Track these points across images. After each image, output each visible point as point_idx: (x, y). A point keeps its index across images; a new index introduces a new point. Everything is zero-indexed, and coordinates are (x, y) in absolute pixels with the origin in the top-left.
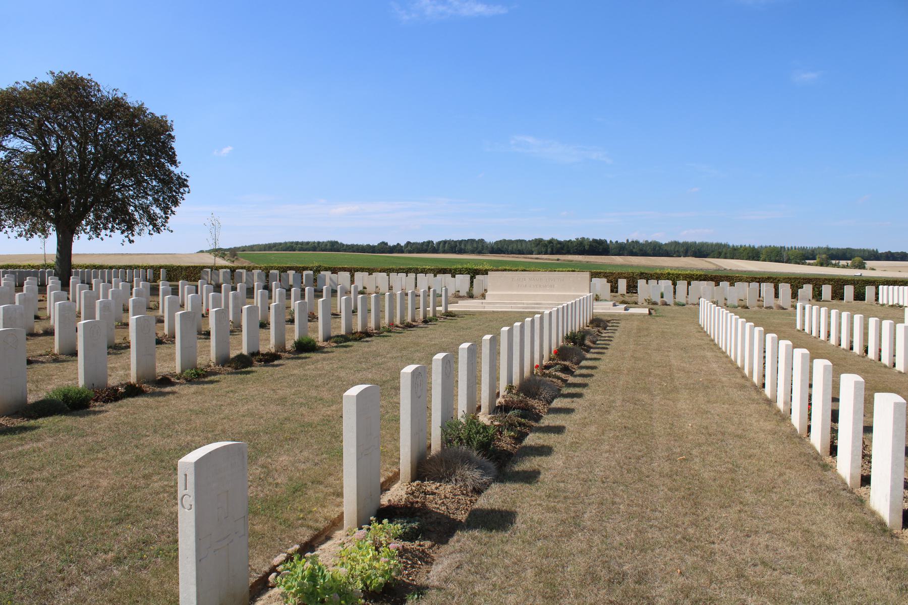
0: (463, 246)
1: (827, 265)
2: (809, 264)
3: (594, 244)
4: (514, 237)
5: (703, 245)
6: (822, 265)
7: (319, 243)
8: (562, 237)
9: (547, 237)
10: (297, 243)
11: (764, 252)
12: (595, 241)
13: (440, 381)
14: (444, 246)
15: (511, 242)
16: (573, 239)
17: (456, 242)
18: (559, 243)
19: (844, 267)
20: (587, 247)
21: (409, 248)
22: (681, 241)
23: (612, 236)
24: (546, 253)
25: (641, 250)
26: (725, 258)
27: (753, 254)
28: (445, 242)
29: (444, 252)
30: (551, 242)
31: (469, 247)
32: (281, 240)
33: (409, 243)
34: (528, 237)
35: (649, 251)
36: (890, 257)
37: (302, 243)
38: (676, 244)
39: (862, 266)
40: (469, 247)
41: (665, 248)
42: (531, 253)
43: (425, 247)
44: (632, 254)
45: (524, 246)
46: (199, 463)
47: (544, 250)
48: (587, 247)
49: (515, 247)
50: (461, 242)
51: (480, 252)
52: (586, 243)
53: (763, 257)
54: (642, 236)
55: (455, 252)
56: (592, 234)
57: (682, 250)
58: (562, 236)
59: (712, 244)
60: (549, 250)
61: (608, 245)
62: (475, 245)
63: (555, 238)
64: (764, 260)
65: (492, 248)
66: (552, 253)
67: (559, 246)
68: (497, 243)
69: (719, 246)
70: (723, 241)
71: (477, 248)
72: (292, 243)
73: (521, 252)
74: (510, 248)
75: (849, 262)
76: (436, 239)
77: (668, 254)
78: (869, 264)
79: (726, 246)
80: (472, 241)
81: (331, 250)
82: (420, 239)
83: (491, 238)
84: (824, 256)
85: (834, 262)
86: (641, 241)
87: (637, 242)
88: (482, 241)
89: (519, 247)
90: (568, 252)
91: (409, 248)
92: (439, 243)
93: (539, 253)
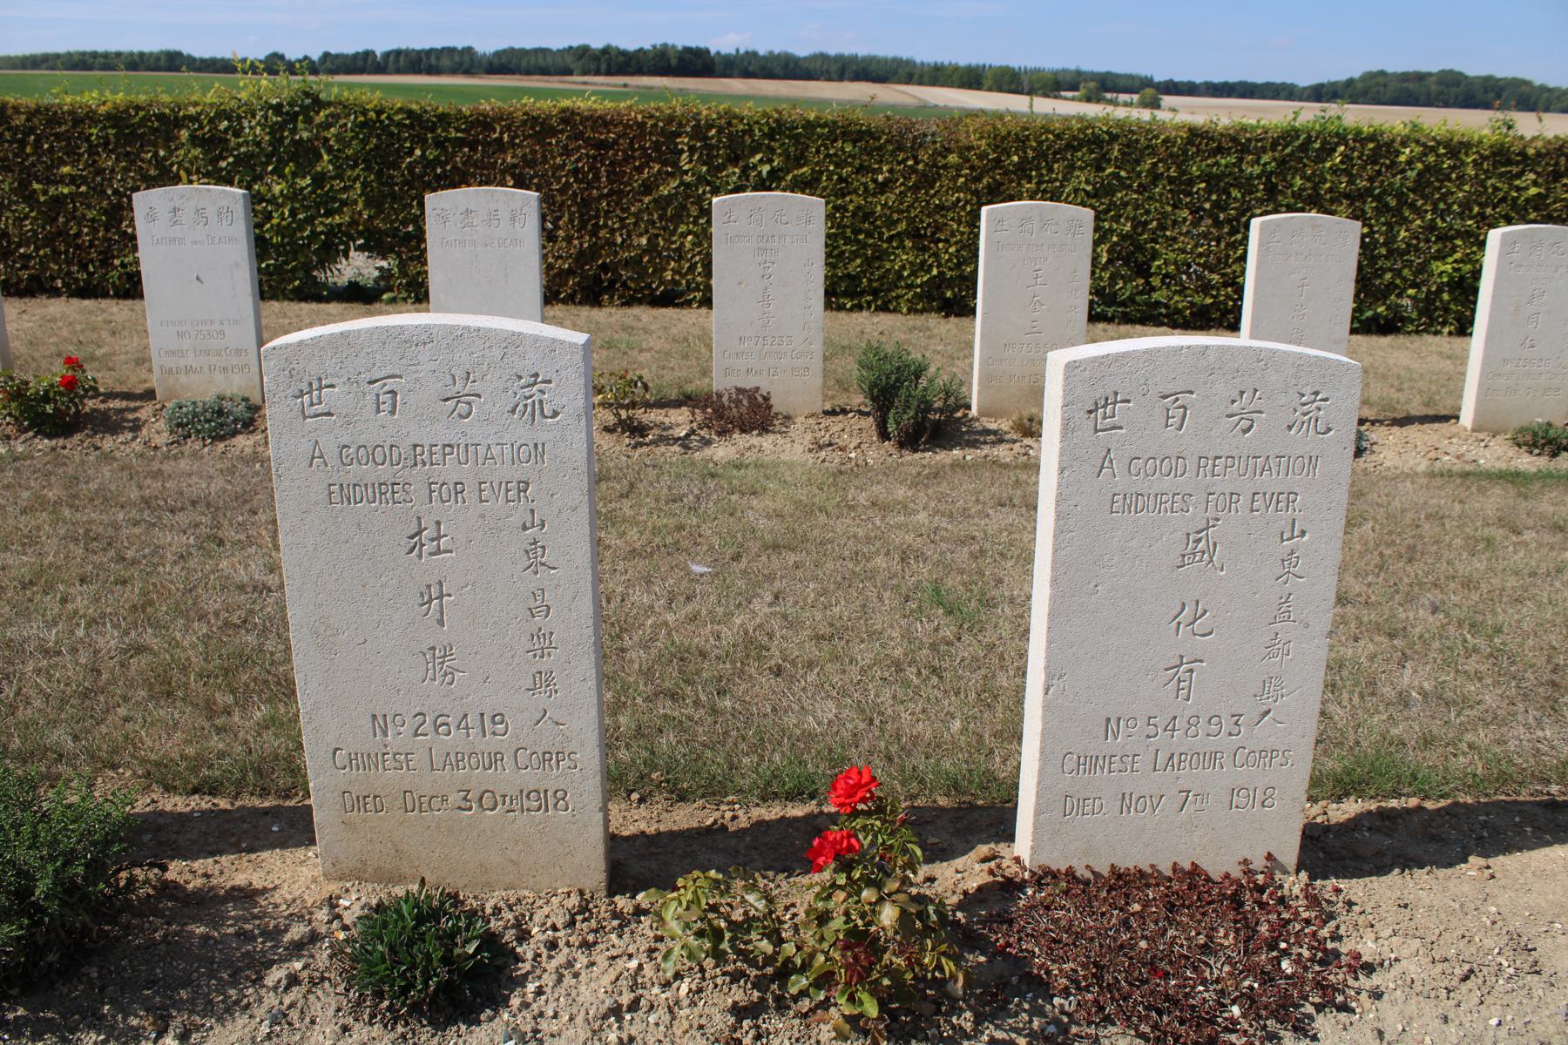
0: (433, 61)
1: (1098, 101)
2: (1066, 99)
3: (687, 56)
4: (529, 44)
5: (871, 60)
6: (1088, 100)
7: (142, 54)
8: (629, 44)
9: (597, 44)
10: (95, 55)
11: (989, 74)
12: (687, 50)
13: (452, 316)
14: (397, 61)
15: (524, 53)
16: (647, 46)
17: (419, 52)
18: (624, 53)
19: (1126, 105)
20: (674, 62)
21: (328, 64)
22: (832, 52)
23: (723, 43)
24: (597, 73)
25: (763, 68)
26: (921, 83)
27: (972, 78)
28: (398, 53)
29: (398, 72)
30: (606, 51)
31: (446, 62)
32: (61, 47)
33: (326, 55)
34: (557, 43)
35: (778, 70)
36: (1190, 89)
37: (106, 55)
38: (824, 57)
39: (1155, 104)
40: (446, 62)
41: (806, 65)
42: (569, 72)
43: (360, 63)
44: (747, 74)
45: (549, 60)
46: (1071, 367)
47: (593, 66)
48: (674, 62)
49: (533, 61)
50: (429, 52)
51: (468, 72)
52: (671, 53)
53: (987, 83)
54: (765, 45)
55: (418, 72)
56: (681, 38)
57: (834, 68)
58: (629, 42)
59: (886, 60)
60: (603, 67)
61: (712, 59)
62: (457, 59)
63: (614, 44)
64: (990, 90)
65: (491, 64)
66: (609, 73)
67: (621, 59)
68: (498, 54)
69: (898, 62)
70: (904, 54)
71: (461, 64)
72: (84, 54)
73: (544, 71)
74: (524, 64)
75: (1136, 97)
76: (380, 48)
77: (809, 75)
78: (1167, 100)
79: (909, 63)
80: (451, 51)
81: (169, 69)
82: (348, 46)
83: (486, 46)
84: (1092, 85)
85: (1108, 96)
86: (762, 52)
87: (755, 54)
88: (469, 51)
89: (541, 61)
90: (640, 72)
91: (328, 64)
92: (387, 55)
93: (585, 73)
